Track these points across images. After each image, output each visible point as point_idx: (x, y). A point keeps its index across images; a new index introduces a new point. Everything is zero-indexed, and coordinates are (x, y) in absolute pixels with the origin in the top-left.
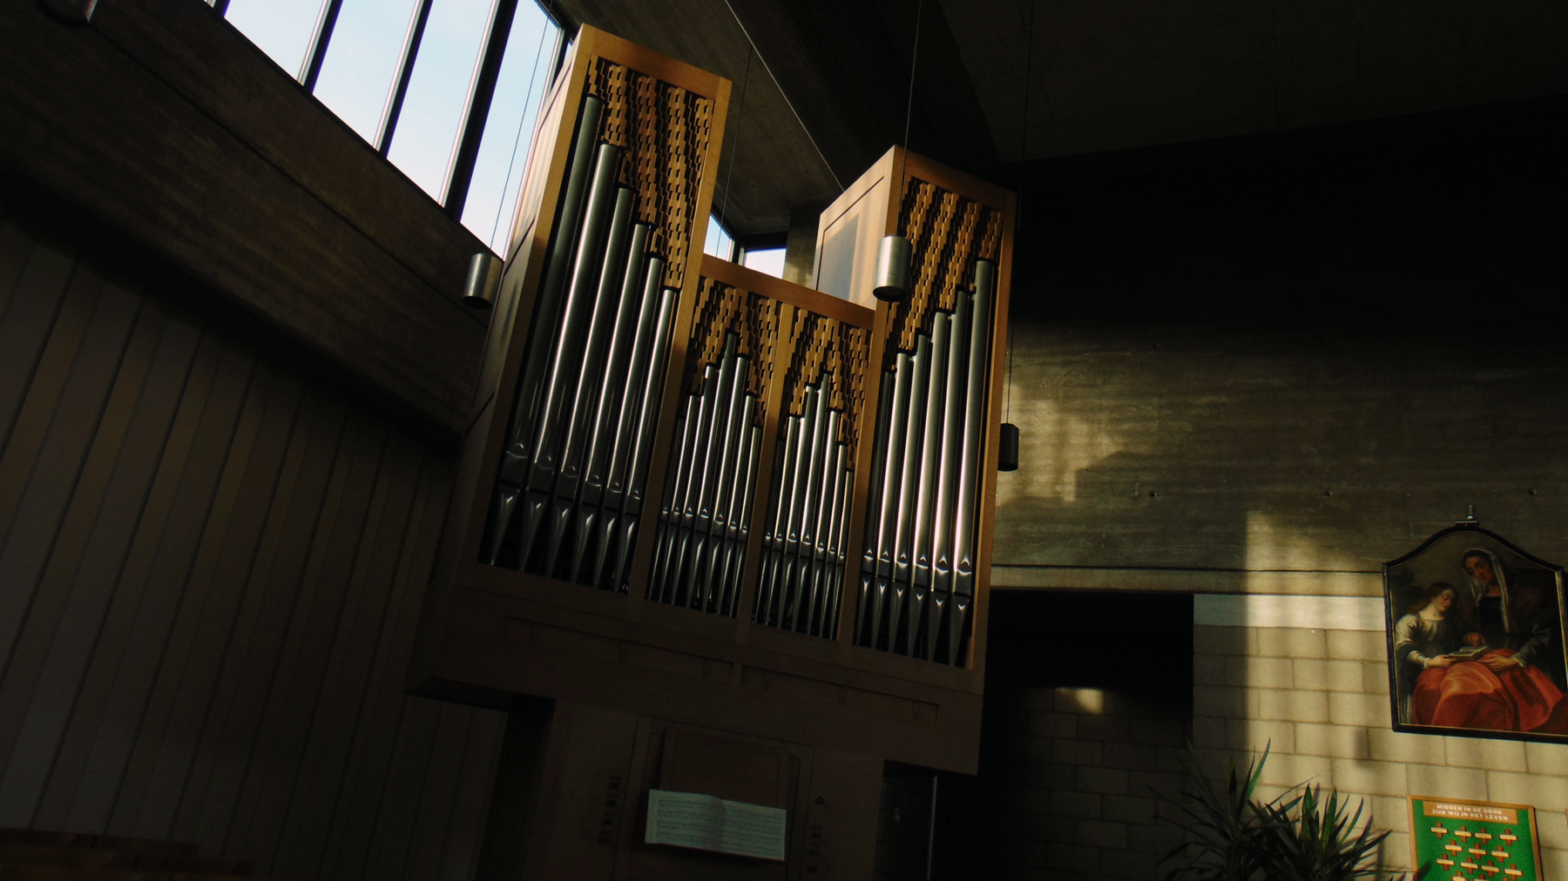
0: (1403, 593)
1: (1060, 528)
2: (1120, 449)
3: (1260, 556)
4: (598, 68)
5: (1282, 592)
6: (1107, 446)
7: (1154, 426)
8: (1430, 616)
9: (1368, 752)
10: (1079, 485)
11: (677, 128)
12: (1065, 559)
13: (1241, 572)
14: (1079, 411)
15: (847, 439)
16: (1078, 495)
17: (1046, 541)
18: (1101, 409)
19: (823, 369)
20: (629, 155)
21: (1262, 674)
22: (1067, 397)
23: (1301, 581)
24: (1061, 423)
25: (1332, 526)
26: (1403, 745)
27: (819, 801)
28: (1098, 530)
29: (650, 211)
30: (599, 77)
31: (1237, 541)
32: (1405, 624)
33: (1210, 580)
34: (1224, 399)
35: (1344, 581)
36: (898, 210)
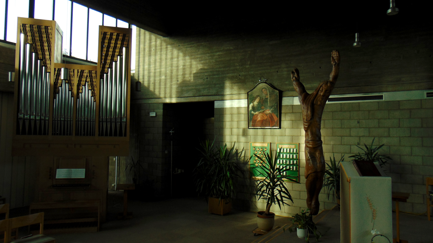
0: (250, 99)
1: (190, 88)
2: (202, 67)
3: (227, 91)
4: (23, 26)
5: (231, 99)
6: (200, 66)
7: (208, 61)
8: (256, 103)
9: (245, 133)
10: (194, 77)
11: (44, 36)
12: (191, 95)
13: (223, 95)
14: (194, 58)
16: (194, 80)
17: (188, 91)
18: (197, 58)
19: (86, 81)
20: (34, 45)
21: (227, 118)
22: (191, 56)
23: (235, 97)
24: (191, 62)
25: (244, 82)
26: (251, 132)
27: (94, 166)
28: (197, 88)
29: (40, 56)
30: (23, 29)
31: (222, 88)
32: (251, 105)
33: (217, 97)
34: (221, 53)
36: (101, 41)
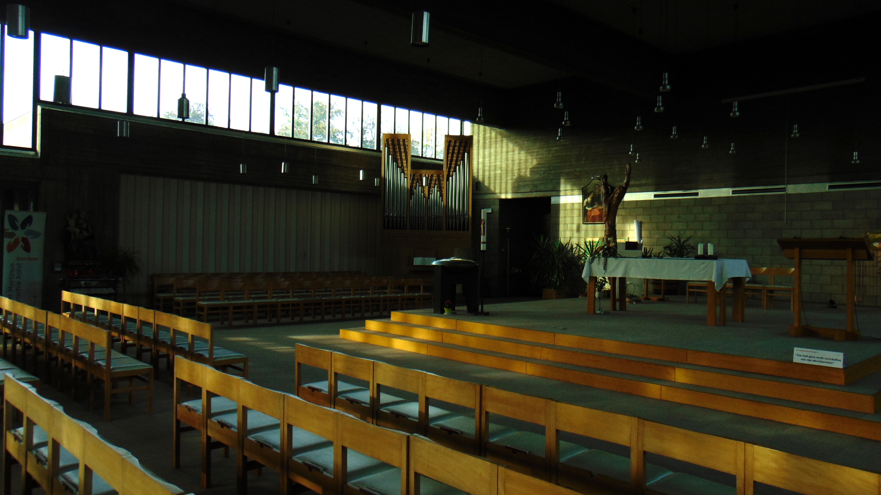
0: (585, 197)
8: (589, 199)
10: (531, 172)
13: (559, 191)
15: (441, 195)
21: (562, 214)
26: (583, 227)
31: (559, 184)
33: (554, 193)
35: (576, 192)
